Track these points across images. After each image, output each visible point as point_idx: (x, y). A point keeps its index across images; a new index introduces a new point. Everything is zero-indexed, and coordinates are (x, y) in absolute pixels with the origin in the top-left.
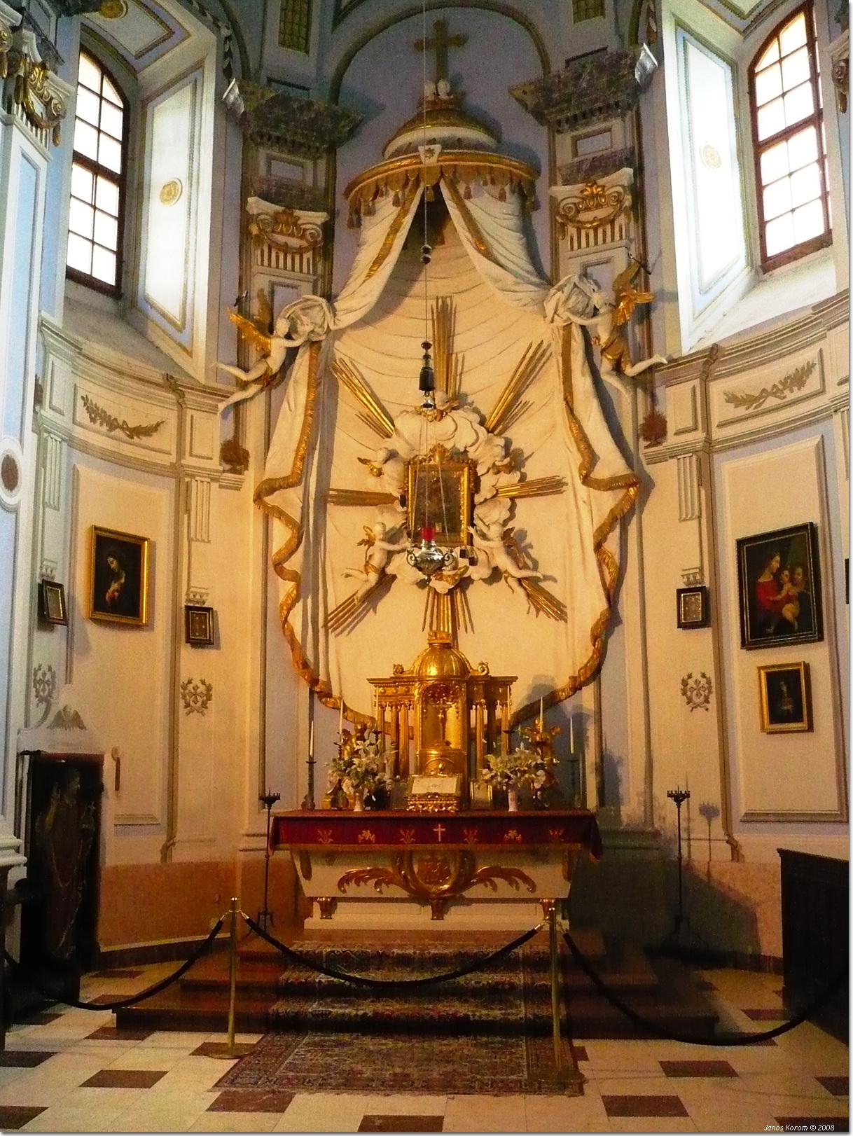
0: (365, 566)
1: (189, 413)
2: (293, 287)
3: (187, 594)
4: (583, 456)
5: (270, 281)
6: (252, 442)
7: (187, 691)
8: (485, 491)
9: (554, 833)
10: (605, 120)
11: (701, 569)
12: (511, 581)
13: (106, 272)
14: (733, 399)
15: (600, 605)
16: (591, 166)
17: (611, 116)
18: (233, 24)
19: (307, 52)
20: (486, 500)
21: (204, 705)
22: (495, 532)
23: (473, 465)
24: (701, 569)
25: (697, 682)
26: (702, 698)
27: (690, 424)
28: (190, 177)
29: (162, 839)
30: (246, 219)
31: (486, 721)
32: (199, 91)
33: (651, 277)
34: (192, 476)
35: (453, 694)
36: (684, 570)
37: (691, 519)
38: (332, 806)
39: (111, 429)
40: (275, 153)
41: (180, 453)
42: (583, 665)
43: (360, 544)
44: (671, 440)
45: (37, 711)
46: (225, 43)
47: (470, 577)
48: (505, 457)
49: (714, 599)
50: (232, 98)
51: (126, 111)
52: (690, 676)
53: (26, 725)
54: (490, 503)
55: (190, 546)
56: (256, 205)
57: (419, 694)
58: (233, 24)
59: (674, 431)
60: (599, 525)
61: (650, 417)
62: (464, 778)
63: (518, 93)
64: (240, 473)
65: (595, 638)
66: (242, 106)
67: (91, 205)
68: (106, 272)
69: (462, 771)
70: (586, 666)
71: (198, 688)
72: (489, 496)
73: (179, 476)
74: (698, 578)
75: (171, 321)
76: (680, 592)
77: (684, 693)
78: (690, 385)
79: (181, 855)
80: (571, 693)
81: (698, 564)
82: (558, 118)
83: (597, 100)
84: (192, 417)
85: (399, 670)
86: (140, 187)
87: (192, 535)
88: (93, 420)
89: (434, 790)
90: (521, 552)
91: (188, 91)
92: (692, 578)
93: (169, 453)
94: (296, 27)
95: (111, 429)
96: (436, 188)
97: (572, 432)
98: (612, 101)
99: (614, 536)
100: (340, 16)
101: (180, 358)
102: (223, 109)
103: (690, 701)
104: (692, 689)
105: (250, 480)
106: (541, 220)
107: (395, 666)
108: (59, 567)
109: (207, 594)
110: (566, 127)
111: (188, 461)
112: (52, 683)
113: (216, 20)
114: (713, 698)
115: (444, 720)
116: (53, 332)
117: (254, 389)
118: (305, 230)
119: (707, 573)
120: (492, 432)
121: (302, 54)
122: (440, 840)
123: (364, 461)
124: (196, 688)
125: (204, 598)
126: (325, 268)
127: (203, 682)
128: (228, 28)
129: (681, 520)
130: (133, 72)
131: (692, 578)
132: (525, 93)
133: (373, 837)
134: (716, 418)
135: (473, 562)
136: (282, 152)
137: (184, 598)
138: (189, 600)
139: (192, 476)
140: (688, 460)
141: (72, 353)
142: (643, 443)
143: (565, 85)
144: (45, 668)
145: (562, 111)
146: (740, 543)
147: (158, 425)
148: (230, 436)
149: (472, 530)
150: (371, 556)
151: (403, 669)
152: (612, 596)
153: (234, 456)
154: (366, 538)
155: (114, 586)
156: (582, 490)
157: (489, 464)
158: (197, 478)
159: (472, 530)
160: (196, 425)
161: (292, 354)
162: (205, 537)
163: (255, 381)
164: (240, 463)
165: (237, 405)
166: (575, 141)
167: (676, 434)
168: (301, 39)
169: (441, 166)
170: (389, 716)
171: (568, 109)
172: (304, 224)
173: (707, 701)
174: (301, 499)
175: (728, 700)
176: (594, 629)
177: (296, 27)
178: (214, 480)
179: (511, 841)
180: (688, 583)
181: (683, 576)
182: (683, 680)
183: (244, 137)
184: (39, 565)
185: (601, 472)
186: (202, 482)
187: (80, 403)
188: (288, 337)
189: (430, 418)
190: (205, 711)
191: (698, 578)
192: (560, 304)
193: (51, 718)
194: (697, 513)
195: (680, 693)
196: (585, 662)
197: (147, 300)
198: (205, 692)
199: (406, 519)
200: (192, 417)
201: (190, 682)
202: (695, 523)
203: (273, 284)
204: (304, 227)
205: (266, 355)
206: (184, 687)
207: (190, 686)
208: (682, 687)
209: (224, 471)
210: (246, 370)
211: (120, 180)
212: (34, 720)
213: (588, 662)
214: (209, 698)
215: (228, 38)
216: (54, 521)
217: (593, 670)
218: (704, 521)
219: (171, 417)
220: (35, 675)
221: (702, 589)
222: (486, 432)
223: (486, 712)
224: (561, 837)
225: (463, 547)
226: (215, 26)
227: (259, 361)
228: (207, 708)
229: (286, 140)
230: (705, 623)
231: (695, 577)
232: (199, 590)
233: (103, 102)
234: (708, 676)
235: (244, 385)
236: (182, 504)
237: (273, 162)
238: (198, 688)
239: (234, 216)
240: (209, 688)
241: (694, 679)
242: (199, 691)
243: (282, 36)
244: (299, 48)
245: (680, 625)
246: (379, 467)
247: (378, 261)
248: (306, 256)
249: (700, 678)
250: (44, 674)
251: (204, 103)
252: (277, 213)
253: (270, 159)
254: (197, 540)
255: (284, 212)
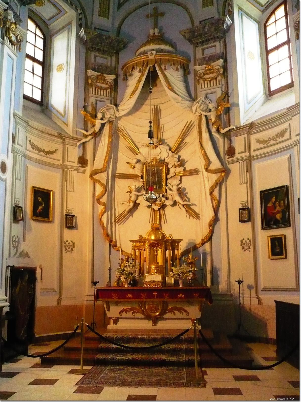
0: (129, 200)
1: (67, 146)
2: (103, 101)
3: (66, 210)
4: (206, 161)
5: (95, 99)
6: (89, 156)
7: (66, 245)
8: (171, 174)
9: (195, 295)
10: (214, 42)
11: (247, 201)
12: (180, 205)
13: (37, 96)
14: (259, 141)
15: (212, 214)
16: (208, 59)
17: (216, 41)
18: (82, 8)
19: (108, 18)
20: (171, 177)
21: (72, 249)
22: (175, 188)
23: (167, 165)
24: (247, 201)
25: (246, 241)
26: (248, 247)
27: (243, 150)
28: (67, 62)
29: (57, 297)
30: (87, 78)
31: (171, 255)
32: (70, 32)
33: (230, 98)
34: (68, 169)
35: (160, 246)
36: (241, 202)
37: (244, 184)
38: (117, 285)
39: (39, 152)
40: (97, 54)
41: (64, 160)
42: (206, 235)
43: (127, 192)
44: (237, 156)
45: (13, 252)
46: (80, 15)
47: (166, 204)
48: (178, 162)
49: (252, 212)
50: (82, 35)
51: (45, 39)
52: (243, 239)
53: (9, 256)
54: (173, 178)
55: (67, 193)
56: (90, 72)
57: (148, 246)
58: (82, 8)
59: (238, 153)
60: (211, 186)
61: (229, 147)
62: (164, 275)
63: (183, 33)
64: (85, 167)
65: (210, 226)
66: (86, 37)
67: (32, 73)
68: (37, 96)
69: (163, 273)
70: (207, 236)
71: (70, 243)
72: (172, 176)
73: (63, 168)
74: (246, 204)
75: (60, 114)
76: (240, 209)
77: (241, 245)
78: (243, 136)
79: (64, 303)
80: (201, 245)
81: (246, 200)
82: (197, 42)
83: (211, 35)
84: (68, 147)
85: (141, 237)
86: (50, 66)
87: (68, 189)
88: (33, 149)
89: (153, 280)
90: (184, 195)
91: (66, 32)
92: (244, 205)
93: (60, 160)
94: (104, 10)
95: (39, 152)
96: (154, 67)
97: (202, 153)
98: (216, 36)
99: (217, 190)
100: (120, 6)
101: (63, 127)
102: (79, 39)
103: (243, 248)
104: (244, 244)
105: (88, 170)
106: (191, 78)
107: (139, 236)
108: (21, 201)
109: (73, 210)
110: (200, 45)
111: (66, 163)
112: (18, 242)
113: (76, 7)
114: (252, 247)
115: (157, 255)
116: (19, 117)
117: (90, 138)
118: (108, 81)
119: (249, 203)
120: (174, 153)
121: (106, 19)
122: (155, 297)
123: (128, 163)
124: (69, 243)
125: (72, 212)
126: (115, 95)
127: (72, 242)
128: (80, 10)
129: (240, 184)
130: (47, 25)
131: (244, 205)
132: (185, 33)
133: (132, 296)
134: (253, 148)
135: (167, 199)
136: (99, 54)
137: (65, 211)
138: (67, 212)
139: (68, 169)
140: (243, 163)
141: (25, 125)
142: (227, 157)
143: (200, 30)
144: (16, 236)
145: (198, 39)
146: (261, 192)
147: (56, 150)
148: (81, 154)
149: (166, 188)
150: (131, 197)
151: (142, 237)
152: (216, 211)
153: (83, 161)
154: (129, 190)
155: (40, 207)
156: (206, 174)
157: (173, 164)
158: (70, 169)
159: (166, 188)
160: (69, 150)
161: (103, 125)
162: (72, 190)
163: (90, 135)
164: (85, 164)
165: (84, 143)
166: (203, 50)
167: (238, 154)
168: (106, 14)
169: (156, 59)
170: (137, 254)
171: (201, 38)
172: (107, 79)
173: (249, 248)
174: (106, 177)
175: (257, 248)
176: (209, 222)
177: (104, 10)
178: (75, 170)
179: (180, 298)
180: (243, 206)
181: (241, 204)
182: (241, 241)
183: (86, 48)
184: (14, 200)
185: (212, 167)
186: (71, 170)
187: (28, 142)
188: (102, 119)
189: (152, 148)
190: (72, 252)
191: (246, 204)
192: (198, 107)
193: (18, 254)
194: (246, 182)
195: (240, 245)
196: (207, 234)
197: (52, 106)
198: (72, 245)
199: (143, 184)
200: (68, 147)
201: (67, 241)
202: (245, 185)
203: (96, 101)
204: (107, 80)
205: (94, 126)
206: (65, 243)
207: (67, 243)
208: (241, 243)
209: (79, 167)
210: (87, 131)
211: (42, 64)
212: (12, 255)
213: (208, 234)
214: (74, 247)
215: (81, 13)
216: (19, 184)
217: (209, 237)
218: (248, 184)
219: (60, 147)
220: (12, 239)
221: (248, 208)
222: (171, 153)
223: (171, 252)
224: (198, 296)
225: (163, 194)
226: (76, 9)
227: (91, 128)
228: (73, 250)
229: (101, 50)
230: (249, 220)
231: (245, 204)
232: (70, 209)
233: (36, 36)
234: (250, 239)
235: (86, 136)
236: (64, 178)
237: (96, 57)
238: (70, 243)
239: (83, 76)
240: (74, 244)
241: (245, 240)
242: (70, 244)
243: (99, 13)
244: (105, 17)
245: (240, 221)
246: (134, 165)
247: (133, 92)
248: (108, 91)
249: (247, 240)
250: (16, 239)
251: (72, 36)
252: (98, 75)
253: (95, 56)
254: (70, 191)
255: (100, 75)
